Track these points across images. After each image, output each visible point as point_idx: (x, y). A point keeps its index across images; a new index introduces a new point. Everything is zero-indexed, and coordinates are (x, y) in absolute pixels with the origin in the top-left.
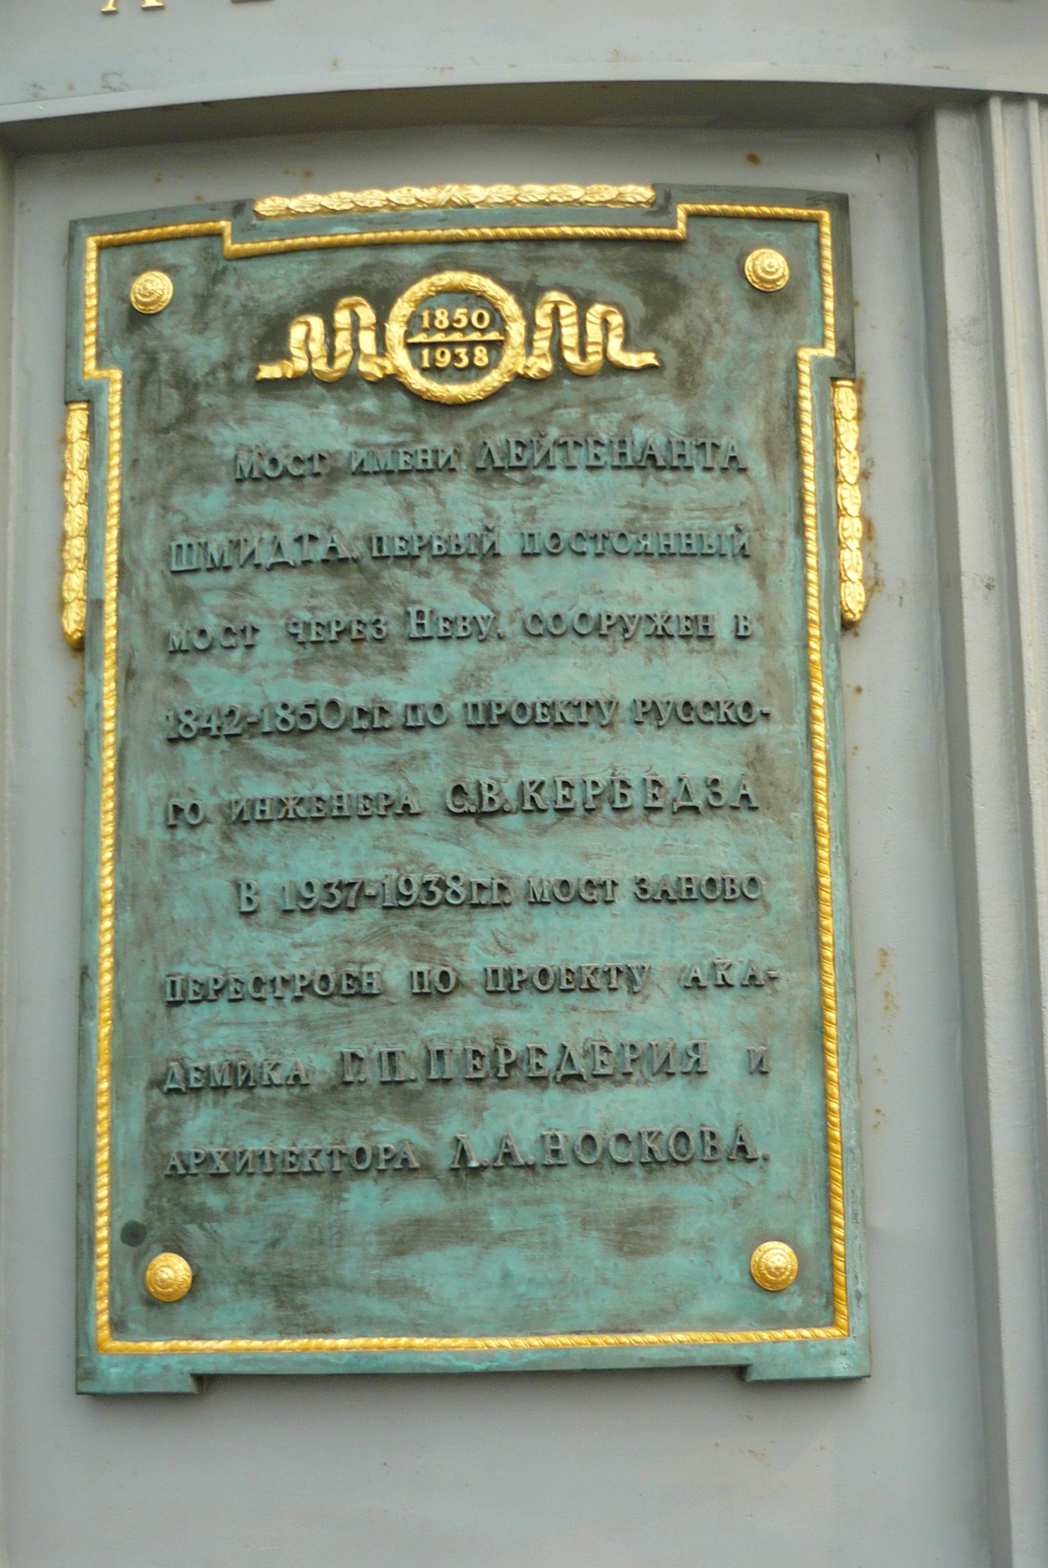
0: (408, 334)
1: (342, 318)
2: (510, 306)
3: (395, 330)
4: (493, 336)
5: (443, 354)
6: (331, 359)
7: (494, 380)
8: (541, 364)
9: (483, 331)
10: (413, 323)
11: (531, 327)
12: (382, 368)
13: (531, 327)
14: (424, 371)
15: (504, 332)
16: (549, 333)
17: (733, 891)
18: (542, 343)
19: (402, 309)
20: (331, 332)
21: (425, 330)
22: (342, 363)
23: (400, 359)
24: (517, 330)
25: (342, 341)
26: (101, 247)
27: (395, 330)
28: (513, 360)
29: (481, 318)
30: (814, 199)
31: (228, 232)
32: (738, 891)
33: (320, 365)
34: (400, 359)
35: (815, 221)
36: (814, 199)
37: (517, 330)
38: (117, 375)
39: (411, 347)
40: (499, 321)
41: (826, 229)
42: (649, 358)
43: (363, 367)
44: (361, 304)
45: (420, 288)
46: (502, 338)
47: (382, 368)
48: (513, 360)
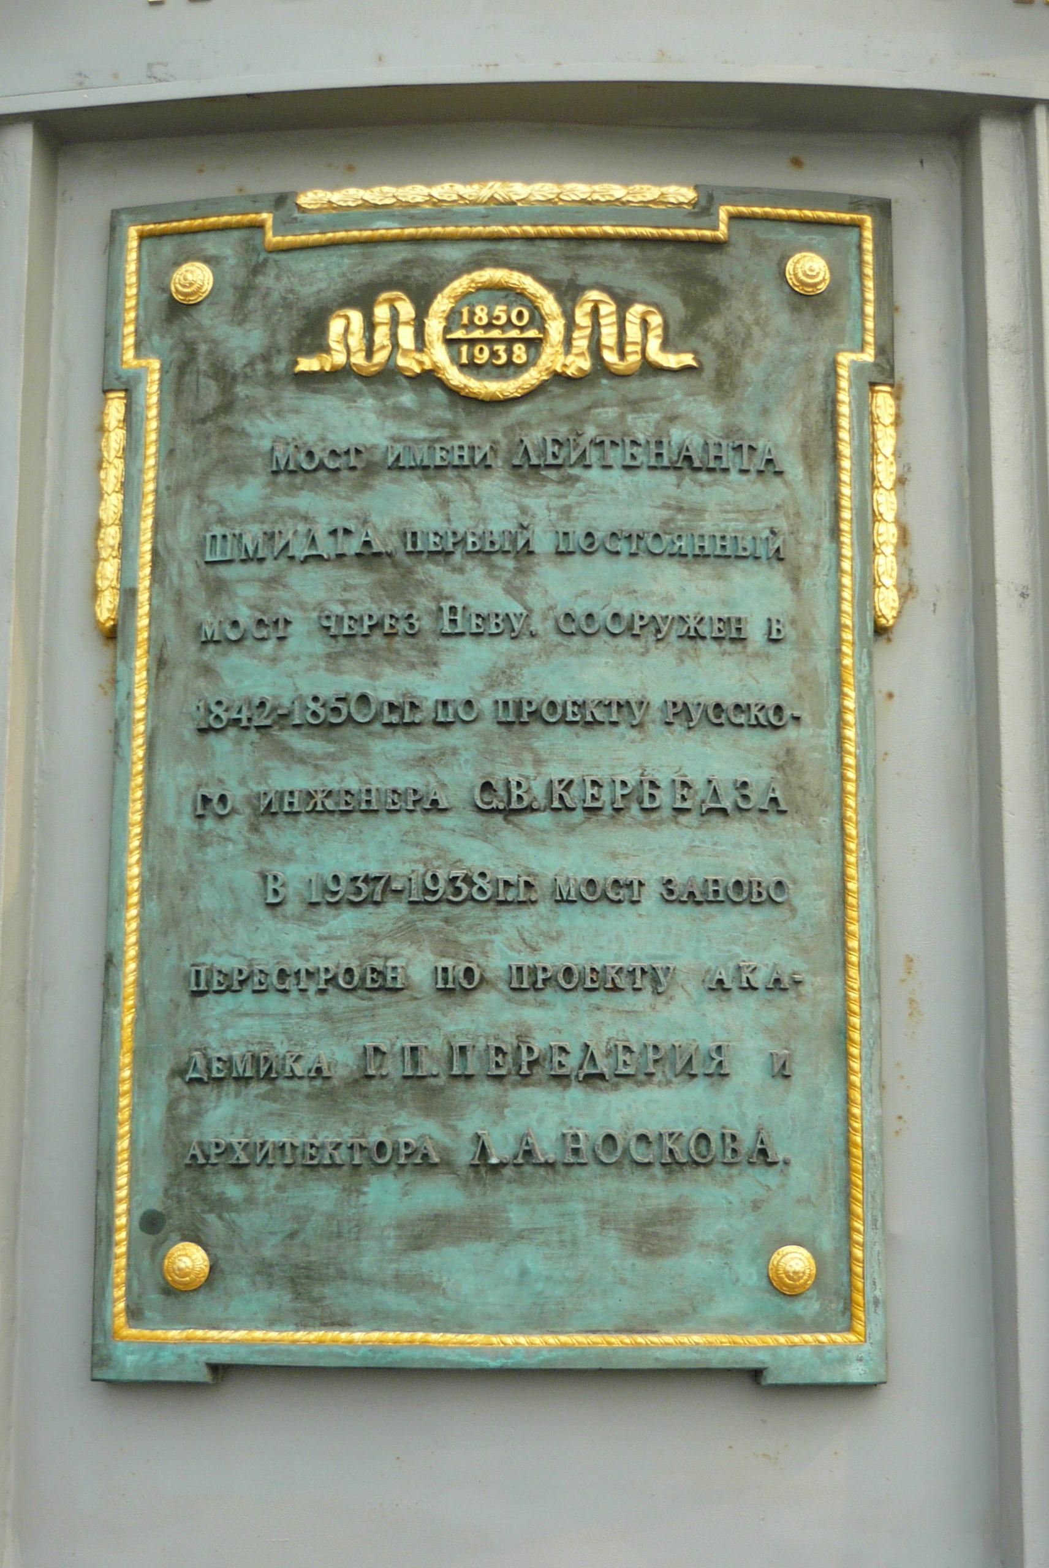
0: (447, 330)
1: (381, 312)
2: (549, 304)
3: (434, 326)
4: (532, 333)
5: (481, 350)
6: (369, 353)
7: (531, 377)
8: (579, 363)
9: (522, 329)
10: (452, 319)
11: (571, 325)
12: (421, 363)
13: (571, 325)
14: (462, 367)
15: (543, 330)
16: (588, 331)
17: (760, 894)
18: (581, 342)
19: (442, 304)
20: (370, 326)
21: (465, 326)
22: (380, 357)
23: (439, 355)
24: (556, 328)
25: (381, 336)
26: (142, 237)
27: (434, 326)
28: (552, 358)
29: (520, 315)
30: (856, 204)
31: (269, 224)
32: (765, 895)
33: (359, 359)
34: (439, 355)
35: (858, 226)
36: (856, 204)
37: (556, 328)
38: (156, 364)
39: (450, 343)
40: (538, 319)
41: (868, 234)
42: (688, 359)
43: (401, 362)
44: (400, 299)
45: (461, 285)
46: (541, 336)
47: (421, 363)
48: (552, 358)
